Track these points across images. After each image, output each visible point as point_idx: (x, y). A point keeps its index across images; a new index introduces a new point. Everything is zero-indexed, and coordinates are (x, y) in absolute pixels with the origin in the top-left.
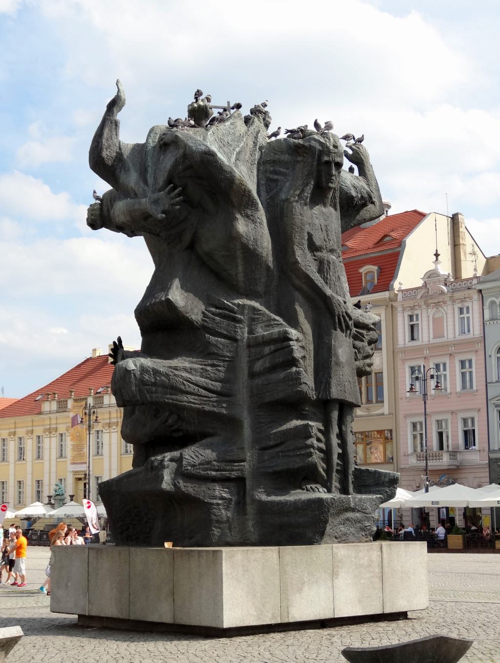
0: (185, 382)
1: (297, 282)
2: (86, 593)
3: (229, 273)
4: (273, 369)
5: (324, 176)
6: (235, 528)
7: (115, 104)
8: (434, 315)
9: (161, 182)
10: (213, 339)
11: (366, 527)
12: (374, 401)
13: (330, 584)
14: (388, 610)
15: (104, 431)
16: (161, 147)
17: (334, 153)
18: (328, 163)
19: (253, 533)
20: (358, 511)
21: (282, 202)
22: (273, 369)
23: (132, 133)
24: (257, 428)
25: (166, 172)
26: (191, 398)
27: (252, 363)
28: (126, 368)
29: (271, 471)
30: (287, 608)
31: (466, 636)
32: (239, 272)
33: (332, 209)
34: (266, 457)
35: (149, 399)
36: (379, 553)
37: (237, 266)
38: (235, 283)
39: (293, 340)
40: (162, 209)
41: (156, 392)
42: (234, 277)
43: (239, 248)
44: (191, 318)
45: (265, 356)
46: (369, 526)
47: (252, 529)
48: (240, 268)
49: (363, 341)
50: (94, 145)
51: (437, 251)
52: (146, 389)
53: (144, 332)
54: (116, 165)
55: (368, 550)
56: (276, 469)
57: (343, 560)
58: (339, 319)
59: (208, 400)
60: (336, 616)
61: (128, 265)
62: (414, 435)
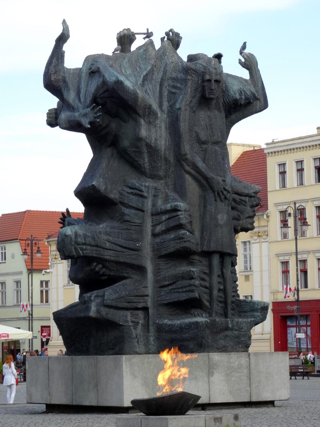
0: (105, 242)
1: (187, 168)
2: (47, 388)
3: (139, 164)
4: (168, 230)
5: (207, 90)
7: (62, 39)
9: (88, 101)
13: (207, 380)
14: (254, 399)
15: (253, 241)
16: (90, 74)
17: (175, 97)
18: (209, 81)
19: (154, 345)
20: (236, 330)
21: (177, 110)
22: (168, 230)
23: (74, 60)
24: (157, 272)
25: (91, 94)
27: (154, 226)
28: (65, 234)
29: (166, 302)
31: (201, 396)
32: (145, 161)
33: (216, 112)
34: (163, 293)
35: (82, 254)
36: (248, 359)
37: (144, 159)
38: (143, 170)
40: (89, 121)
41: (86, 250)
42: (142, 166)
43: (144, 146)
44: (111, 197)
45: (162, 222)
46: (245, 340)
47: (153, 343)
48: (146, 160)
50: (46, 71)
52: (80, 248)
53: (85, 205)
54: (61, 85)
55: (238, 358)
57: (217, 364)
58: (218, 193)
59: (123, 254)
60: (211, 402)
61: (75, 153)
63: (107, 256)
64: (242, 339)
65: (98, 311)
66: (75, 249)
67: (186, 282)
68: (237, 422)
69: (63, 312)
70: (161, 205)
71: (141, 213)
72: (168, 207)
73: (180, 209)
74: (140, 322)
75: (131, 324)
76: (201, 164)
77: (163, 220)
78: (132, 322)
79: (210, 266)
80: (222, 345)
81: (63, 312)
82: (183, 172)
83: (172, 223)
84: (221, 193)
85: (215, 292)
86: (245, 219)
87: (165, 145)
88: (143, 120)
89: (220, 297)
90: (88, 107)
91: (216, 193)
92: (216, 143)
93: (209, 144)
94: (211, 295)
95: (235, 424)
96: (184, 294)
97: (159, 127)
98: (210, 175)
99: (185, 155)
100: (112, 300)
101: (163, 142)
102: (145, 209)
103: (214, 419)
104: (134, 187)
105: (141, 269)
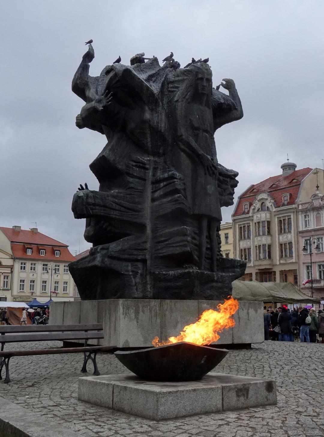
3: (143, 143)
4: (166, 195)
6: (139, 289)
7: (89, 57)
8: (316, 215)
10: (131, 180)
11: (225, 292)
12: (288, 256)
14: (236, 342)
18: (202, 79)
20: (220, 282)
23: (96, 70)
26: (117, 213)
27: (154, 192)
30: (166, 337)
33: (207, 108)
35: (91, 213)
37: (147, 139)
39: (176, 178)
41: (95, 209)
43: (148, 127)
47: (149, 290)
48: (149, 139)
49: (227, 185)
51: (317, 185)
52: (90, 207)
56: (165, 254)
58: (208, 168)
62: (266, 245)
63: (113, 214)
64: (225, 290)
65: (103, 261)
66: (86, 208)
67: (179, 239)
68: (271, 394)
69: (76, 263)
70: (160, 175)
71: (143, 182)
72: (166, 175)
73: (176, 177)
74: (139, 271)
75: (131, 273)
76: (193, 143)
77: (161, 187)
78: (132, 271)
79: (200, 229)
80: (209, 294)
81: (76, 263)
82: (179, 150)
83: (169, 189)
84: (210, 169)
85: (204, 249)
86: (227, 195)
87: (165, 127)
88: (147, 107)
89: (208, 254)
90: (102, 95)
91: (206, 168)
92: (206, 131)
93: (201, 131)
94: (200, 251)
95: (268, 397)
96: (178, 248)
97: (160, 113)
98: (201, 152)
99: (182, 135)
100: (116, 252)
101: (163, 125)
102: (147, 178)
103: (236, 391)
104: (138, 161)
105: (142, 227)
